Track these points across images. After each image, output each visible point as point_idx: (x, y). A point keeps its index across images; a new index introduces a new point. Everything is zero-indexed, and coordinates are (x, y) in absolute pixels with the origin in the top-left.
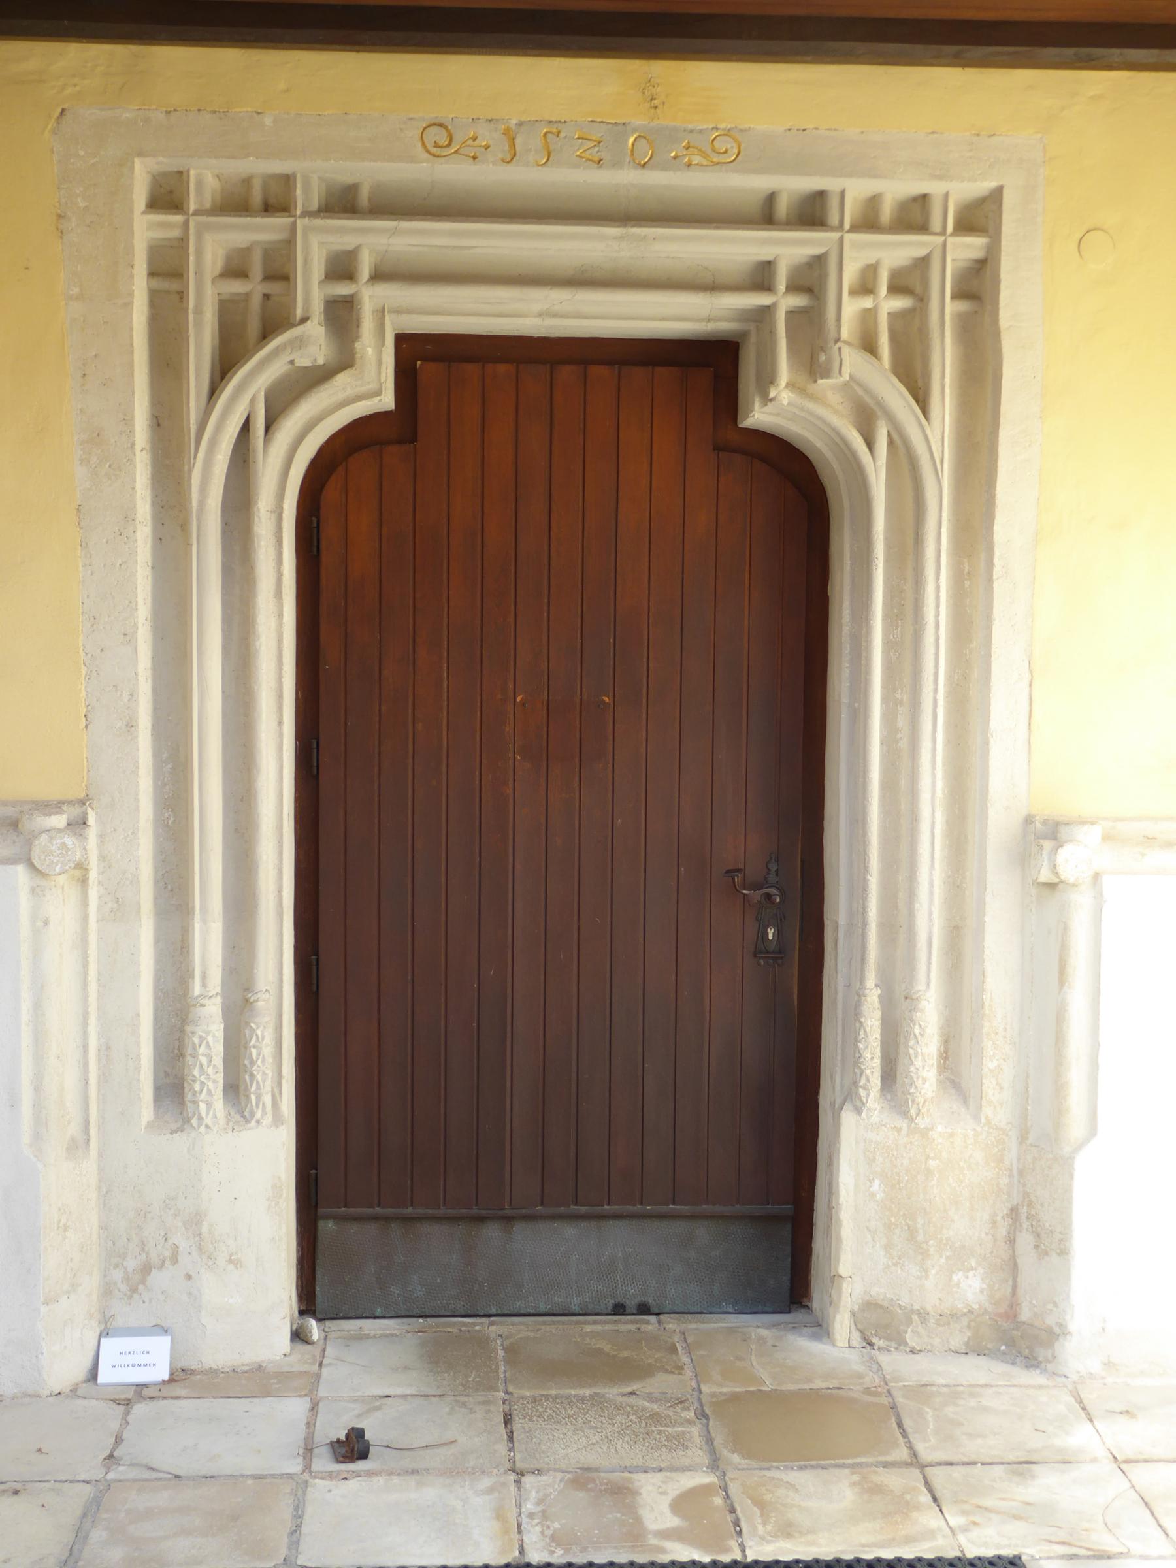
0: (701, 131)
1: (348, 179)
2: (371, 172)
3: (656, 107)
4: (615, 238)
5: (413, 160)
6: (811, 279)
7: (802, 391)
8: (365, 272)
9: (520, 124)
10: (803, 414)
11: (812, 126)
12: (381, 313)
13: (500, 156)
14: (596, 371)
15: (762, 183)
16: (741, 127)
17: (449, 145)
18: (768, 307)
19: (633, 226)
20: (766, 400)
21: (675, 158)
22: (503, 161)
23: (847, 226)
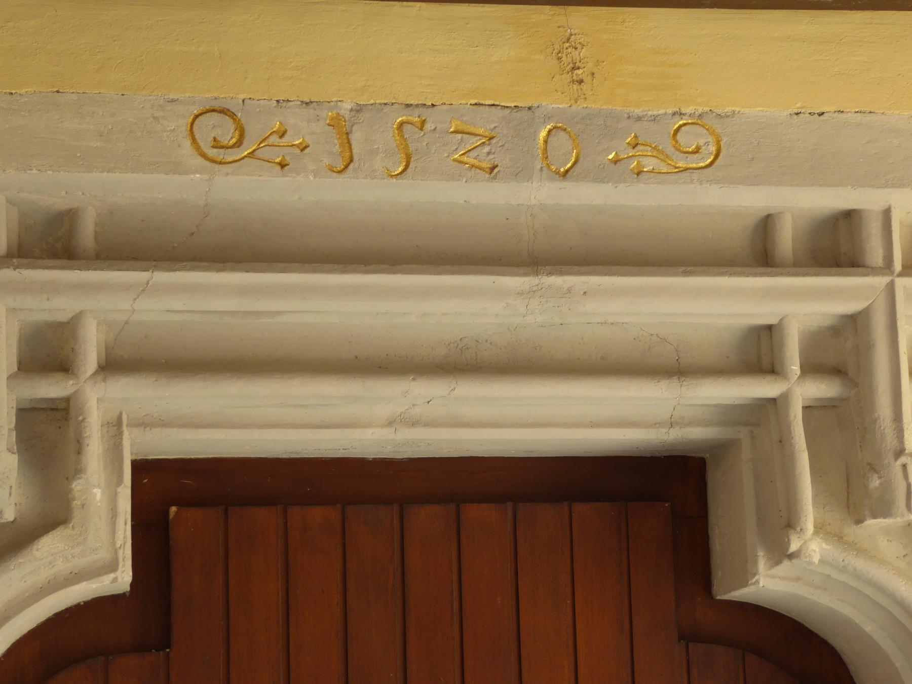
0: (655, 119)
1: (58, 202)
2: (98, 190)
3: (581, 82)
4: (520, 294)
5: (177, 168)
6: (842, 352)
7: (837, 538)
8: (90, 357)
9: (358, 109)
10: (843, 578)
11: (832, 109)
12: (115, 427)
13: (327, 161)
14: (475, 513)
15: (754, 199)
16: (719, 111)
17: (239, 144)
18: (773, 401)
19: (550, 274)
20: (780, 553)
21: (616, 161)
22: (332, 169)
23: (898, 266)
